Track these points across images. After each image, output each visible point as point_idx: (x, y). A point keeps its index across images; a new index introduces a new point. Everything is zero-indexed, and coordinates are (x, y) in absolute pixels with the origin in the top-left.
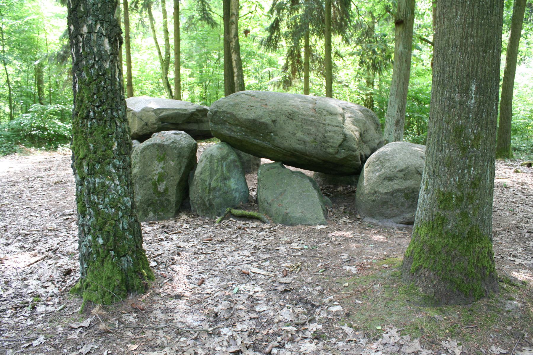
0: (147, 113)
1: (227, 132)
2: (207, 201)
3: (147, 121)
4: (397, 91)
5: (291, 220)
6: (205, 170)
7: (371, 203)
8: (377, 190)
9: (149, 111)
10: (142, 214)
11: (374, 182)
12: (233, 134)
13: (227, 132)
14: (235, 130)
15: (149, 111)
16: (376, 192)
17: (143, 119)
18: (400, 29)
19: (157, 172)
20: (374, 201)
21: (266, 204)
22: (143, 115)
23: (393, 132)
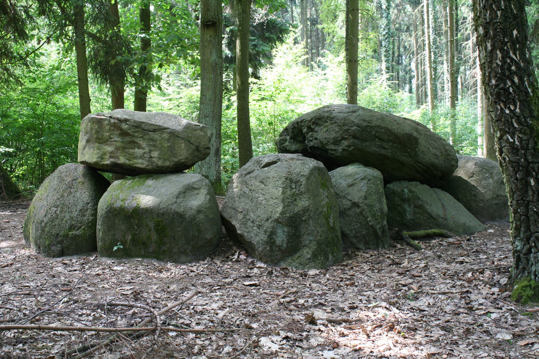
0: (194, 132)
1: (376, 149)
2: (380, 228)
3: (197, 144)
4: (213, 112)
5: (469, 230)
6: (370, 194)
7: (494, 207)
8: (499, 194)
9: (196, 130)
10: (324, 258)
11: (494, 188)
12: (383, 151)
13: (376, 149)
14: (386, 146)
15: (196, 130)
16: (498, 196)
17: (192, 140)
18: (210, 33)
19: (324, 203)
20: (496, 204)
21: (441, 219)
22: (190, 135)
23: (213, 164)
